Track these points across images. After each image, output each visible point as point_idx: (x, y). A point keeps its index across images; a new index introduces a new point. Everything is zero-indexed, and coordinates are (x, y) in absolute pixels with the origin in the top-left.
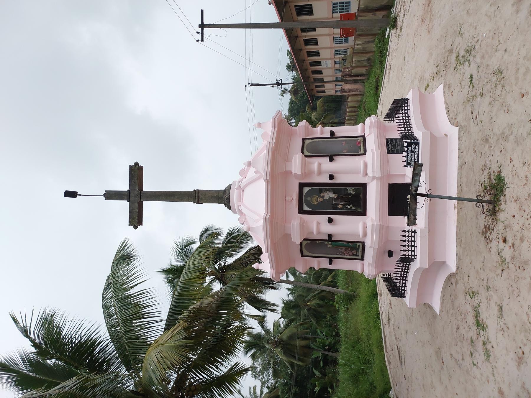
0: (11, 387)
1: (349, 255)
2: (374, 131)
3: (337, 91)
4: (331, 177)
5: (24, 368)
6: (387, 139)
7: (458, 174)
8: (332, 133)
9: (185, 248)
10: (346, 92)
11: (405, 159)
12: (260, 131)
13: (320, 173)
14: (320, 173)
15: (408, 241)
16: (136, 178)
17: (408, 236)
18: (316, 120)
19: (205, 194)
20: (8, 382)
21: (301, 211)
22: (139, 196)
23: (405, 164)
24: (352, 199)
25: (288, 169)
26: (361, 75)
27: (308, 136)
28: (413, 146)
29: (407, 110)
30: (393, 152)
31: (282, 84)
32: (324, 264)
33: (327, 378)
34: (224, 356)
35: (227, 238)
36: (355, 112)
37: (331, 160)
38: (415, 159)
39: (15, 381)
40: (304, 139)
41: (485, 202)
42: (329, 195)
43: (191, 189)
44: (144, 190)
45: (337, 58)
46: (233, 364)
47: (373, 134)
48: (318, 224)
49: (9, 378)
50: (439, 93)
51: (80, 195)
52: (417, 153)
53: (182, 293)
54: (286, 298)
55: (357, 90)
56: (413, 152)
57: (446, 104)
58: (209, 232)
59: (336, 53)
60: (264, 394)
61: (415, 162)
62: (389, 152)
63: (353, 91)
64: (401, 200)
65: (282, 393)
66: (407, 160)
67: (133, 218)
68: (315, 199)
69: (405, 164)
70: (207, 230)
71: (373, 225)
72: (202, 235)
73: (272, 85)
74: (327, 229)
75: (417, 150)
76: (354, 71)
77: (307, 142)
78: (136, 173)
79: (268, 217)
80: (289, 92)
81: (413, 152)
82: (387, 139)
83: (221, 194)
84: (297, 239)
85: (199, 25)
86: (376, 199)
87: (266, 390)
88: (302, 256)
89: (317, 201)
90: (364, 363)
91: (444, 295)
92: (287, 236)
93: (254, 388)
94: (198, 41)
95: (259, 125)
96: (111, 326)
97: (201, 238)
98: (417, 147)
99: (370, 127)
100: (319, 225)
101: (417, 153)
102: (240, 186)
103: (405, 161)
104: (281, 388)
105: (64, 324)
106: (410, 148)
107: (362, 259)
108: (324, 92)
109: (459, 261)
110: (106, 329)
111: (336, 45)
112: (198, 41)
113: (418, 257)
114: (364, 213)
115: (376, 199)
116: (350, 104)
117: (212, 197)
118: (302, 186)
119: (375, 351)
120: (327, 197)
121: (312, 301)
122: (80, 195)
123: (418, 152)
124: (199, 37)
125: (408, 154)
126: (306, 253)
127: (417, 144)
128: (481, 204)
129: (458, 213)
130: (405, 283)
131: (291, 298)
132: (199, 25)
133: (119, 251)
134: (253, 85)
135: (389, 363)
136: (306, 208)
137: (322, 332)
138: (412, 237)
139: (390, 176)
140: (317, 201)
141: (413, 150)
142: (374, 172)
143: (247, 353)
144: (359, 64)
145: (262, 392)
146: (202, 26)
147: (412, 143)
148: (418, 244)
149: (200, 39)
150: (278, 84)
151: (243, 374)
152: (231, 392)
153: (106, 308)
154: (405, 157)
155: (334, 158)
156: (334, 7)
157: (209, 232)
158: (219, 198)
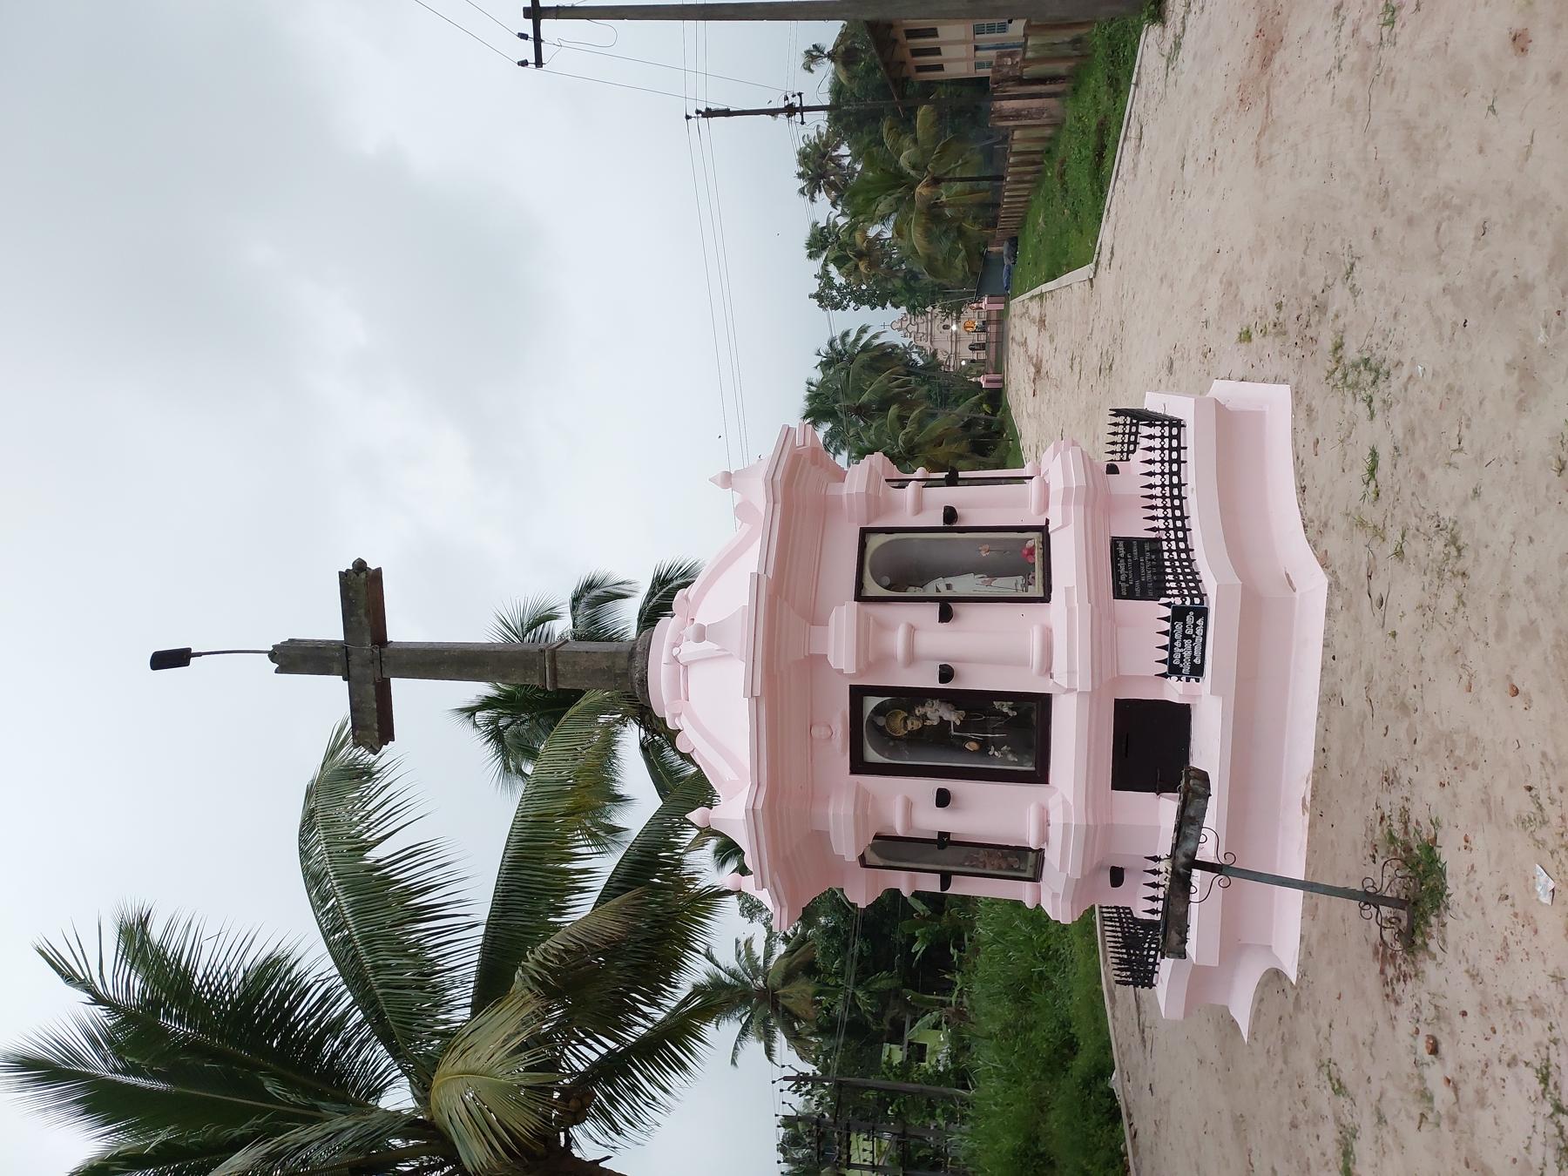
0: (72, 1120)
2: (1076, 513)
3: (979, 65)
4: (946, 673)
5: (99, 1065)
6: (1115, 541)
7: (1319, 716)
8: (950, 514)
9: (529, 630)
10: (1006, 118)
11: (1166, 640)
12: (730, 498)
13: (912, 658)
14: (912, 658)
16: (362, 611)
18: (912, 173)
20: (58, 1107)
21: (859, 766)
22: (377, 663)
23: (1164, 668)
25: (816, 651)
26: (1054, 79)
27: (877, 516)
28: (1190, 619)
29: (1180, 497)
30: (1131, 596)
31: (803, 109)
32: (931, 884)
33: (945, 919)
35: (651, 594)
36: (1034, 163)
37: (946, 616)
38: (1193, 657)
39: (77, 1102)
40: (865, 533)
41: (1387, 901)
42: (936, 713)
44: (391, 636)
47: (1072, 526)
48: (909, 806)
49: (62, 1096)
51: (199, 655)
52: (1199, 640)
53: (526, 853)
55: (1041, 111)
56: (1189, 637)
58: (596, 592)
60: (775, 957)
61: (1192, 664)
62: (1118, 594)
63: (1026, 117)
65: (824, 955)
67: (365, 728)
68: (898, 722)
69: (1164, 668)
70: (590, 586)
71: (1066, 826)
72: (576, 600)
73: (773, 113)
74: (932, 821)
75: (1199, 631)
76: (1029, 71)
77: (875, 541)
78: (362, 590)
79: (759, 806)
80: (829, 56)
81: (1189, 637)
82: (1115, 541)
85: (525, 9)
86: (1076, 740)
87: (781, 949)
89: (905, 727)
90: (1045, 958)
91: (1262, 1000)
92: (820, 839)
93: (748, 943)
94: (524, 63)
95: (727, 479)
96: (331, 928)
97: (573, 608)
98: (1200, 622)
99: (1065, 502)
100: (907, 804)
101: (1199, 640)
102: (676, 658)
103: (1164, 662)
104: (820, 944)
105: (197, 947)
106: (1179, 626)
108: (940, 68)
110: (322, 948)
112: (524, 63)
114: (1040, 775)
115: (1076, 740)
116: (1016, 147)
118: (858, 694)
122: (199, 655)
123: (1204, 636)
125: (1173, 640)
127: (1202, 613)
128: (1374, 910)
129: (1312, 826)
132: (525, 9)
134: (709, 113)
139: (1120, 680)
141: (1189, 632)
142: (1071, 672)
143: (723, 863)
144: (1047, 53)
145: (769, 953)
147: (1188, 609)
149: (532, 59)
150: (790, 110)
152: (683, 1066)
153: (313, 879)
155: (954, 606)
157: (596, 592)
158: (617, 675)
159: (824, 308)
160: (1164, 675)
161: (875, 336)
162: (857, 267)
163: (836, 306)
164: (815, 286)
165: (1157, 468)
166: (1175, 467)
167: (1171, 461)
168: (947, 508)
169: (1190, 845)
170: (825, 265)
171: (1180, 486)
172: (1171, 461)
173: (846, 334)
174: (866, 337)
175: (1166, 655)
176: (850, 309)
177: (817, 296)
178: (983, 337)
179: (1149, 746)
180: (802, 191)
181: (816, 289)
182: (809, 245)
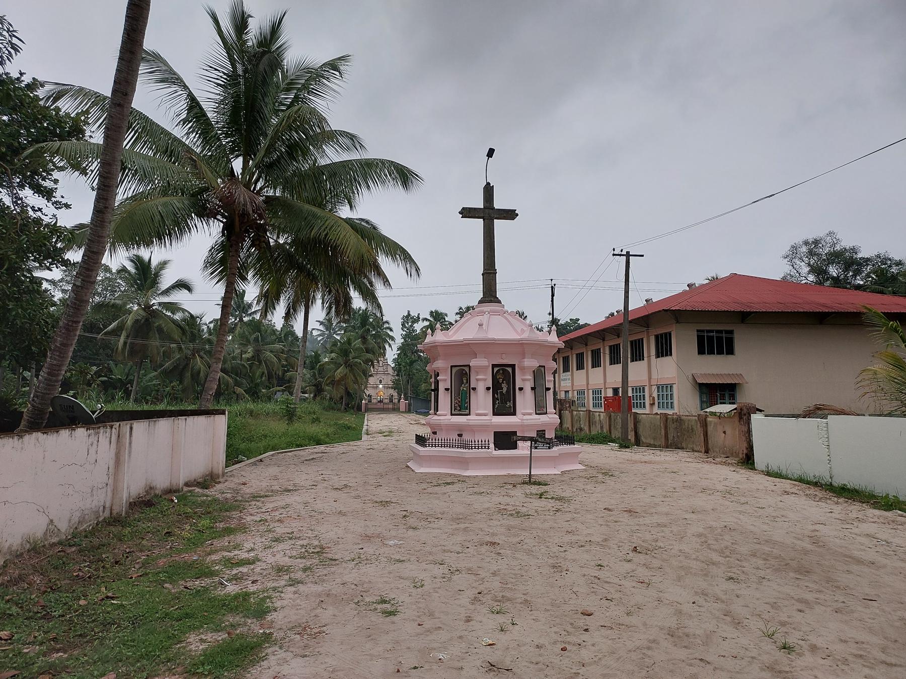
4: (474, 389)
8: (548, 389)
21: (494, 366)
24: (504, 403)
43: (497, 267)
45: (573, 394)
48: (445, 380)
50: (581, 467)
59: (581, 392)
64: (505, 440)
77: (542, 369)
84: (472, 363)
86: (504, 422)
100: (482, 382)
107: (452, 415)
111: (591, 392)
115: (504, 422)
118: (513, 366)
120: (503, 385)
126: (454, 370)
133: (409, 171)
136: (496, 369)
146: (628, 255)
156: (720, 339)
163: (403, 325)
164: (414, 314)
170: (427, 320)
173: (391, 330)
177: (409, 315)
178: (374, 401)
179: (505, 440)
180: (461, 308)
181: (412, 314)
182: (436, 312)
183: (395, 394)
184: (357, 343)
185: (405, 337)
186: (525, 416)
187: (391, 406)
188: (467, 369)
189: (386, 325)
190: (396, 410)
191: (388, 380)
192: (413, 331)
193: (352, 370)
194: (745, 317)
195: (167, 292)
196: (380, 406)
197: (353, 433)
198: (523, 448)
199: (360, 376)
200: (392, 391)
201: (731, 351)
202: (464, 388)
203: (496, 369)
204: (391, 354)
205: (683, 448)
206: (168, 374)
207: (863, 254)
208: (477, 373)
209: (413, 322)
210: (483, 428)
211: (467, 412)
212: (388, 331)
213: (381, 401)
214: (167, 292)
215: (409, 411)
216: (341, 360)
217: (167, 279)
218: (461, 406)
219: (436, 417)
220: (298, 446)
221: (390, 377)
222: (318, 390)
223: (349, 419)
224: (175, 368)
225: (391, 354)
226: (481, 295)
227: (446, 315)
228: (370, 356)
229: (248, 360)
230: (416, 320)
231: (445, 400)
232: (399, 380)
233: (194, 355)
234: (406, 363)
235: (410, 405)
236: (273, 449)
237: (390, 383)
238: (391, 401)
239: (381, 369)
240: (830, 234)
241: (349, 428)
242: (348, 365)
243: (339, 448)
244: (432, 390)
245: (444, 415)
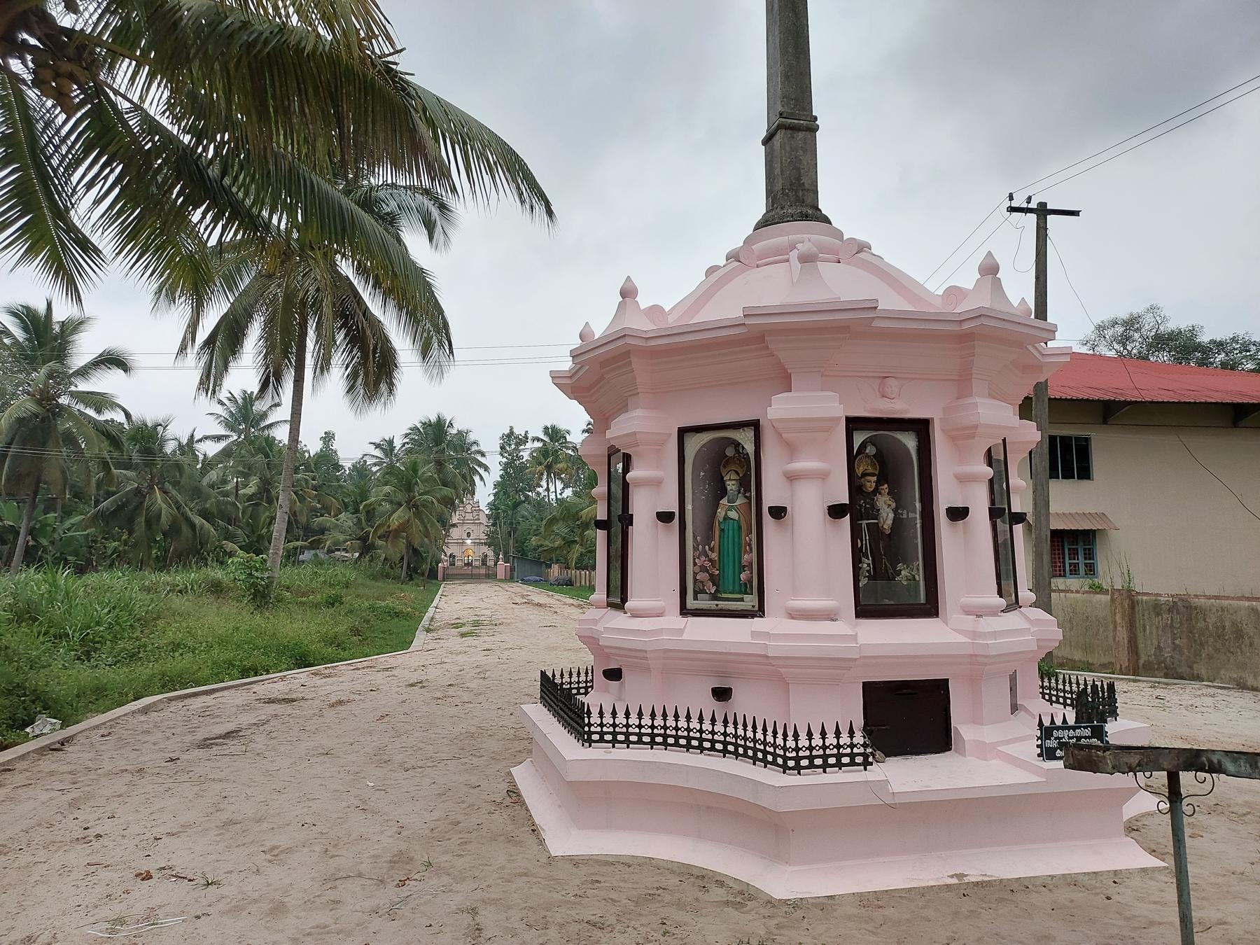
1: (695, 574)
4: (778, 513)
7: (1052, 877)
13: (792, 478)
15: (838, 746)
17: (852, 746)
19: (805, 151)
24: (892, 575)
34: (119, 214)
46: (94, 239)
48: (656, 483)
54: (172, 431)
57: (523, 804)
66: (1058, 728)
69: (1047, 723)
74: (643, 507)
83: (809, 200)
86: (900, 644)
88: (683, 432)
94: (1011, 197)
100: (807, 481)
103: (1053, 722)
109: (815, 905)
112: (1011, 197)
113: (792, 779)
114: (864, 611)
117: (798, 169)
118: (921, 428)
119: (144, 671)
121: (165, 501)
124: (1019, 202)
125: (1074, 728)
126: (695, 444)
130: (676, 744)
131: (170, 447)
135: (145, 711)
136: (859, 438)
137: (75, 526)
138: (811, 758)
140: (864, 475)
143: (14, 314)
146: (1043, 212)
148: (834, 776)
151: (57, 273)
154: (1065, 720)
157: (435, 213)
159: (502, 438)
160: (1041, 724)
161: (482, 478)
162: (540, 464)
163: (502, 448)
165: (608, 719)
166: (646, 739)
167: (614, 734)
168: (784, 509)
169: (1231, 767)
170: (539, 439)
171: (627, 742)
172: (614, 734)
173: (483, 455)
174: (481, 471)
175: (1059, 722)
176: (500, 458)
177: (512, 432)
178: (458, 564)
181: (517, 431)
182: (553, 428)
183: (490, 553)
184: (428, 470)
185: (506, 467)
186: (979, 625)
187: (483, 571)
188: (745, 439)
189: (474, 448)
190: (490, 576)
191: (480, 533)
192: (519, 458)
193: (418, 514)
194: (1108, 412)
195: (83, 372)
196: (468, 570)
197: (392, 631)
198: (986, 751)
199: (433, 525)
200: (485, 549)
201: (1085, 473)
202: (730, 509)
203: (859, 438)
204: (484, 493)
205: (1198, 678)
206: (105, 518)
207: (1204, 338)
208: (792, 450)
209: (518, 444)
210: (822, 671)
211: (750, 601)
212: (479, 458)
213: (468, 564)
214: (83, 372)
215: (511, 578)
216: (400, 497)
217: (84, 349)
218: (726, 576)
219: (618, 620)
220: (245, 673)
221: (483, 528)
222: (366, 547)
223: (403, 596)
224: (120, 508)
225: (484, 493)
226: (759, 208)
227: (568, 432)
228: (447, 491)
229: (250, 498)
230: (524, 440)
231: (654, 555)
232: (495, 532)
233: (151, 487)
234: (507, 505)
235: (512, 569)
236: (164, 688)
237: (483, 536)
238: (484, 562)
239: (469, 516)
240: (1153, 309)
241: (397, 614)
242: (412, 505)
243: (344, 677)
244: (600, 525)
245: (655, 616)
